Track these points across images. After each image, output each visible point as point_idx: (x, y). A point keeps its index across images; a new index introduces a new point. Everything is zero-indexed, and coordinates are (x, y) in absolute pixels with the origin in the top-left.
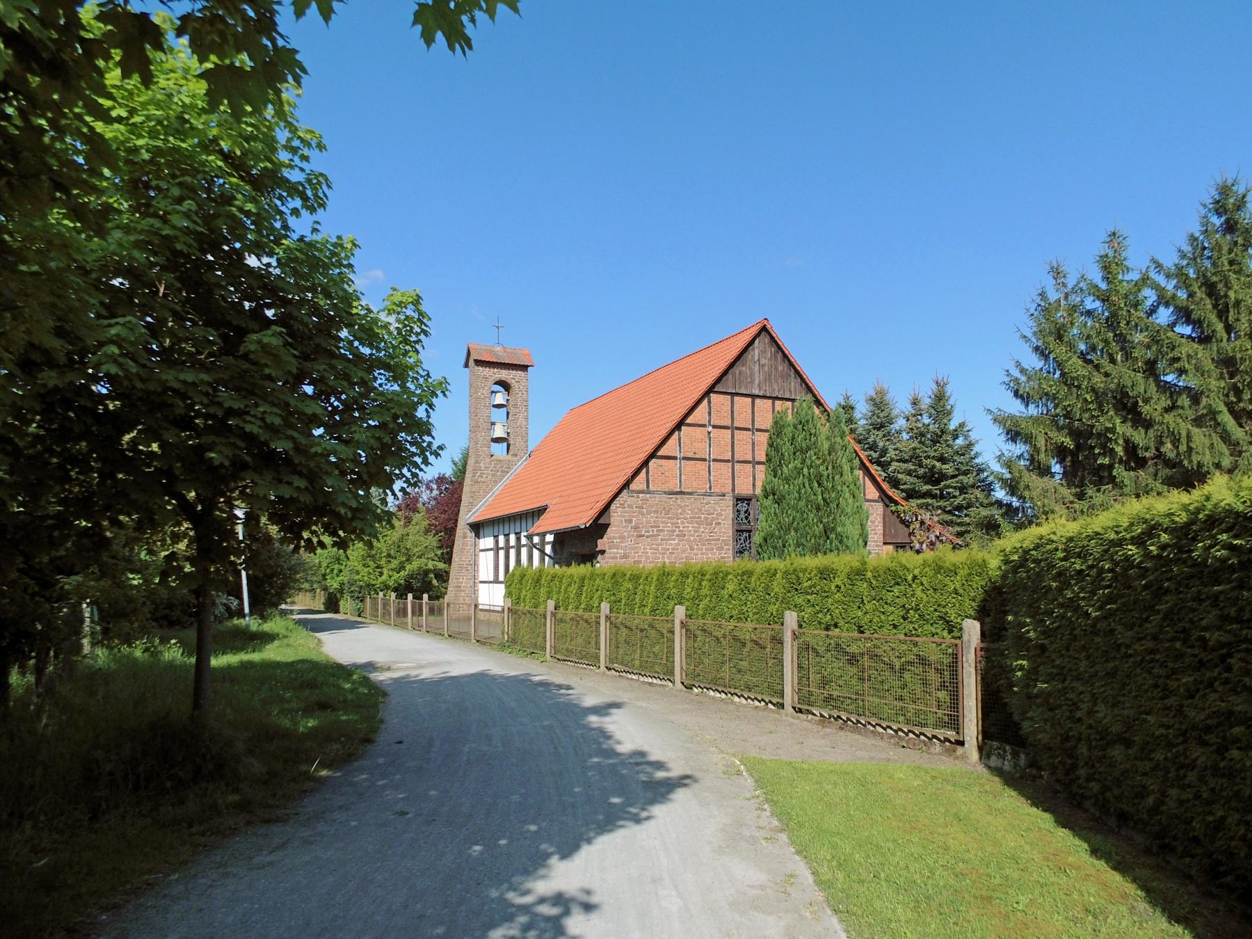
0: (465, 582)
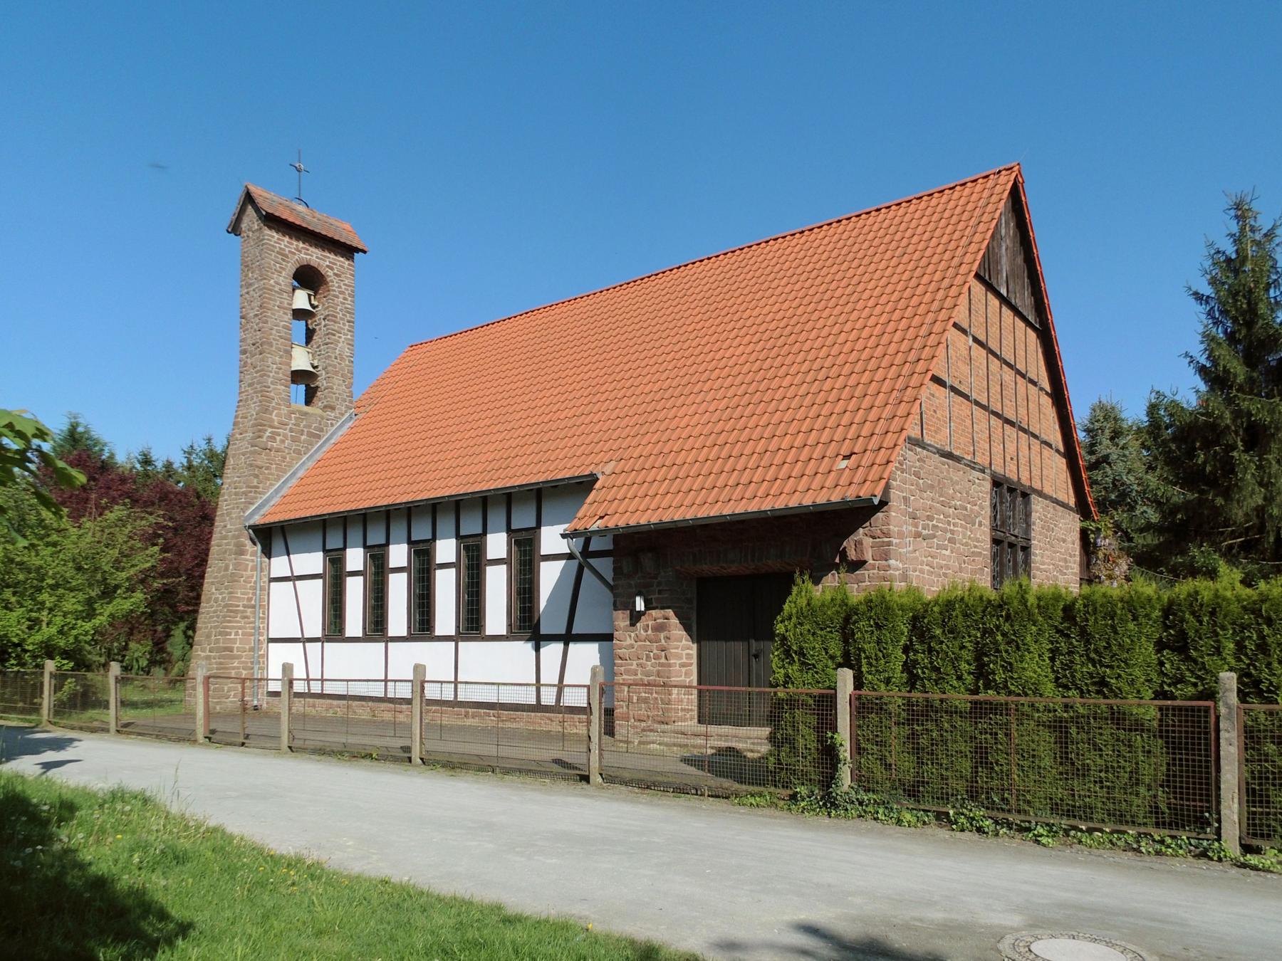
0: (237, 639)
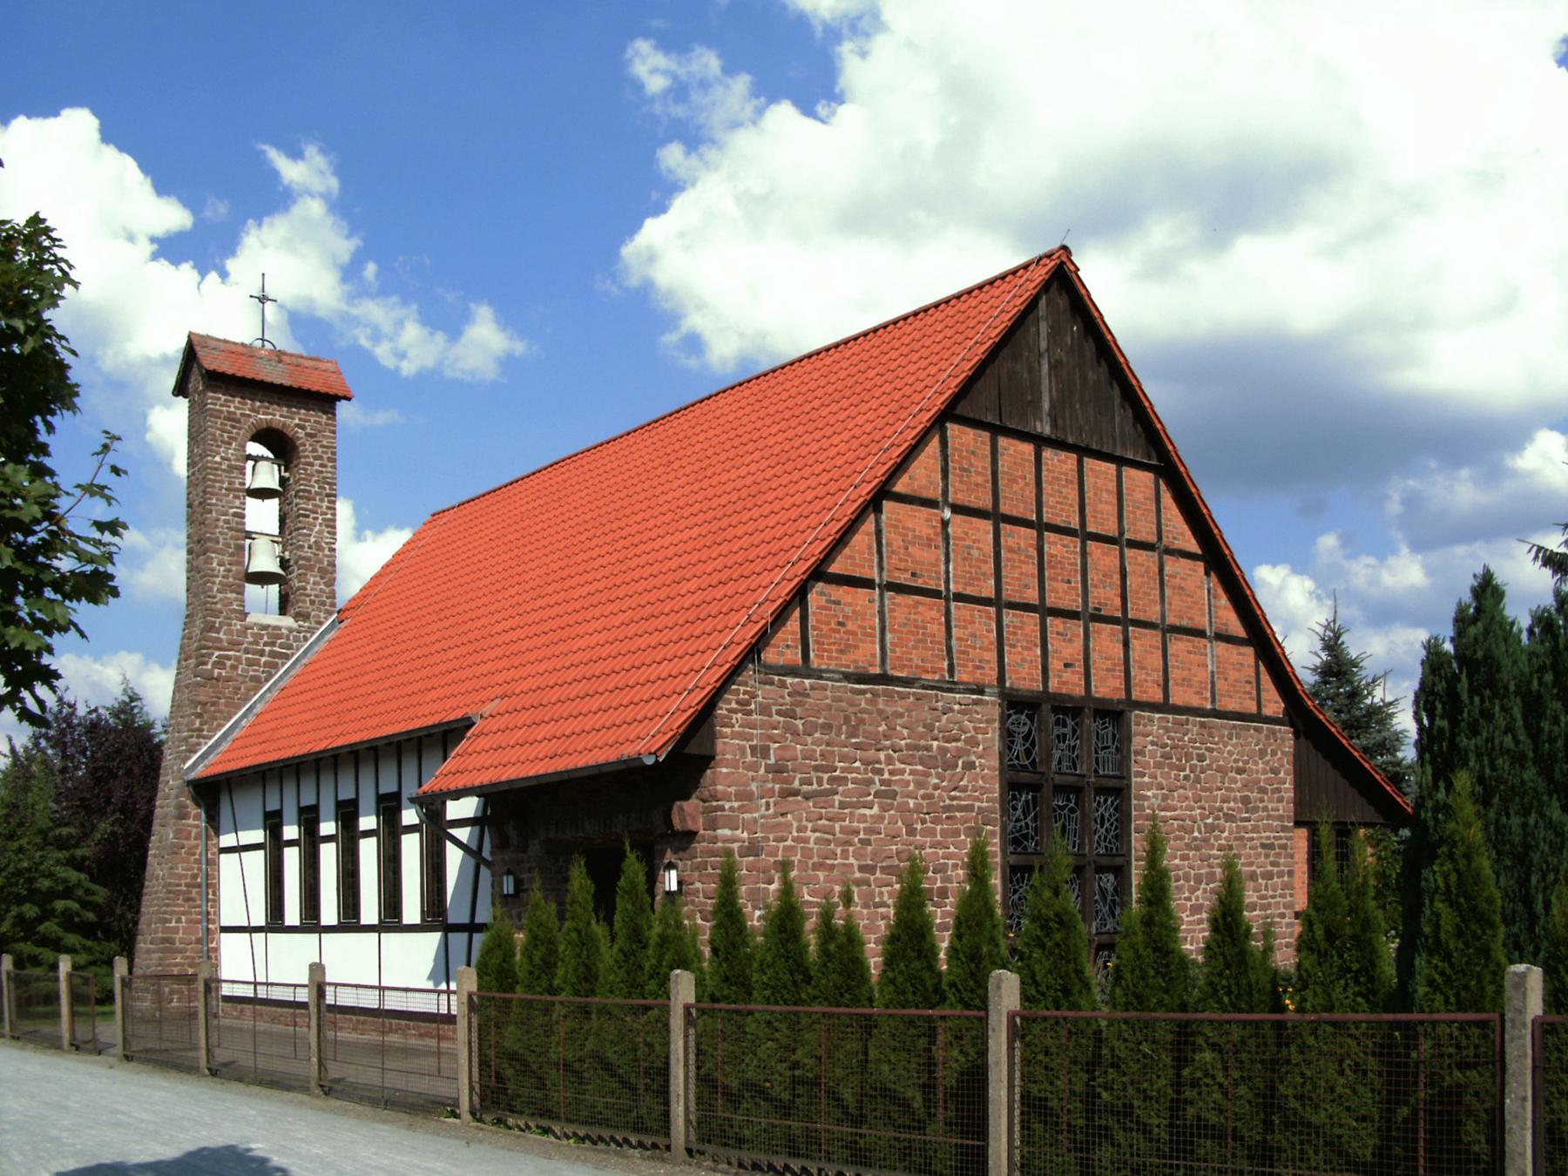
0: (181, 928)
